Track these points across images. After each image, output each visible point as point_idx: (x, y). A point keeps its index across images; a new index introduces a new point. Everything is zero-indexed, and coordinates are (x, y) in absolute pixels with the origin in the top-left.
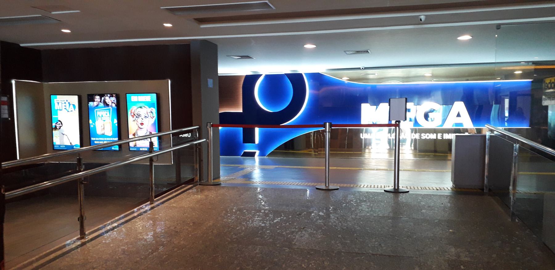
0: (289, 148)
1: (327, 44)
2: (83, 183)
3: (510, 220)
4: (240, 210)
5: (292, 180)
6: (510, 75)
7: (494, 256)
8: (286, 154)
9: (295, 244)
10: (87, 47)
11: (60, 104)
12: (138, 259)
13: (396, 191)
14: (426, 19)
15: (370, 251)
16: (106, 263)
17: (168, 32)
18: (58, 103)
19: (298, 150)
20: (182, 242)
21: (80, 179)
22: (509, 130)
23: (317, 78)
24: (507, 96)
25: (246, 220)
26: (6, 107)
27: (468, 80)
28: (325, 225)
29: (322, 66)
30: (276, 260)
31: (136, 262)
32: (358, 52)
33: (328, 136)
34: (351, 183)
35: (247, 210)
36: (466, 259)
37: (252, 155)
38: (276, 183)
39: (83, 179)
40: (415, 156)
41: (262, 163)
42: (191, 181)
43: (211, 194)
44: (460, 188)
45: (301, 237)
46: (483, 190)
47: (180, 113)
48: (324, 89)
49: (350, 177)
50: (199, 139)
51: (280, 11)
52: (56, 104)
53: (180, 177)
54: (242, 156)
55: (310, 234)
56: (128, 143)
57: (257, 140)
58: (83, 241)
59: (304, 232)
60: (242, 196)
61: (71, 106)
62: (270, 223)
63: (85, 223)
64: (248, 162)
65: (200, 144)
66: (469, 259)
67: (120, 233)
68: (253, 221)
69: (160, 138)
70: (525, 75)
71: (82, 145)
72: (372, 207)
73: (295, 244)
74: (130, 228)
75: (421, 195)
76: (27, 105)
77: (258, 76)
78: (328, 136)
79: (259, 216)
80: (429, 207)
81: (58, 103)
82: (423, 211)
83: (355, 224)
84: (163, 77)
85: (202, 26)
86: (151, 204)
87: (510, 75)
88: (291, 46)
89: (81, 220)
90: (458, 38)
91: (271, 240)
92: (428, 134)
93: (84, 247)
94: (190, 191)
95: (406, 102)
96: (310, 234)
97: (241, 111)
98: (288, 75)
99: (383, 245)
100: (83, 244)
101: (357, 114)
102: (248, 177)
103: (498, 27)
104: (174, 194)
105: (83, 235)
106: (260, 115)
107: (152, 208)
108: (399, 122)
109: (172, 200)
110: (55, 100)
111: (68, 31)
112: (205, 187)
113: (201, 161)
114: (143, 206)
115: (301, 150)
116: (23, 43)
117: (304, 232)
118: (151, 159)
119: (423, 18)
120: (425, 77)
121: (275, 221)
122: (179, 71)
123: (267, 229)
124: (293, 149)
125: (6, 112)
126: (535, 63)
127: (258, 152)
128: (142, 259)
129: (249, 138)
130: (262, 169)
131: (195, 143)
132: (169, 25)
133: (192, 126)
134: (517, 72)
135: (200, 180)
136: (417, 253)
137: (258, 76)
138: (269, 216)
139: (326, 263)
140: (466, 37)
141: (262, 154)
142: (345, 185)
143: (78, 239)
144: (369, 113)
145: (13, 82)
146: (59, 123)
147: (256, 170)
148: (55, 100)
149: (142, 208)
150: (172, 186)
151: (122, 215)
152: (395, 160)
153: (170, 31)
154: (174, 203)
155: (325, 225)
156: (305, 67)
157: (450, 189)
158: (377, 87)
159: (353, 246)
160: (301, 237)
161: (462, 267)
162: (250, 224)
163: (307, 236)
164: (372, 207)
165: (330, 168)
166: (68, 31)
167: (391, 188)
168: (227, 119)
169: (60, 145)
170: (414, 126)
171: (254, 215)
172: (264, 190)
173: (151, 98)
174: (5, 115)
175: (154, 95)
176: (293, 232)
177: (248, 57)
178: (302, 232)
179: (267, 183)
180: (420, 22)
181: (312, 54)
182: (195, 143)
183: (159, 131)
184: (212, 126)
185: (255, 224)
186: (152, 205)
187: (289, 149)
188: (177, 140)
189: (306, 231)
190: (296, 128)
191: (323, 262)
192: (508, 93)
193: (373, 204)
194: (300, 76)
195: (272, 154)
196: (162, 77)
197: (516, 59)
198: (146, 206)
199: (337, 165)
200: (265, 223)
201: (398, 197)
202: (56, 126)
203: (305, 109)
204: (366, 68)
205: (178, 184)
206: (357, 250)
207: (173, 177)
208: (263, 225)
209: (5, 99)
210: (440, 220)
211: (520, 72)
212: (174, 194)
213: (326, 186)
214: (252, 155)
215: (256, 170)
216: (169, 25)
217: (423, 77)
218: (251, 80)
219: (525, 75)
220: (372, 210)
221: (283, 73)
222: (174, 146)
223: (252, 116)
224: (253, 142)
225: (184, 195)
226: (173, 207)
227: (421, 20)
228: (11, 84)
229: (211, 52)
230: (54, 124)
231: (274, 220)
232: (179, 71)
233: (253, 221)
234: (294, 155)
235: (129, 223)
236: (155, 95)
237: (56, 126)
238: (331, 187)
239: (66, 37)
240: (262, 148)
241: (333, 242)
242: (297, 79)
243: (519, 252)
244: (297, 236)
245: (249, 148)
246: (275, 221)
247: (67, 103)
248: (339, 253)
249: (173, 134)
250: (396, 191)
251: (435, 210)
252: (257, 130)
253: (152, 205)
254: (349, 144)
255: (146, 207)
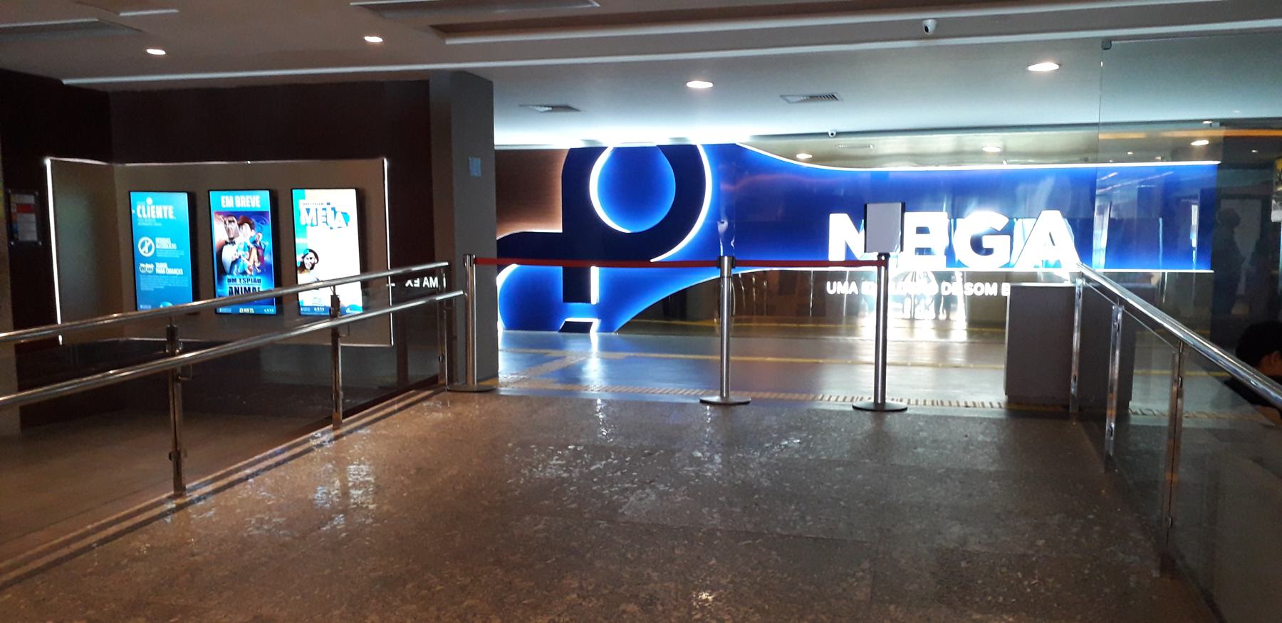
0: (677, 314)
1: (741, 81)
2: (178, 381)
3: (1102, 471)
4: (524, 445)
5: (670, 383)
6: (1180, 150)
7: (1040, 542)
8: (668, 329)
9: (623, 514)
10: (294, 81)
11: (312, 212)
12: (287, 539)
13: (880, 408)
14: (937, 26)
15: (778, 530)
16: (220, 545)
17: (373, 55)
18: (308, 210)
19: (693, 320)
20: (385, 508)
21: (174, 370)
22: (1118, 278)
23: (729, 155)
24: (1195, 197)
25: (530, 464)
26: (33, 217)
27: (1086, 161)
28: (698, 476)
29: (741, 129)
30: (574, 544)
31: (283, 545)
32: (813, 98)
33: (727, 286)
34: (809, 392)
35: (538, 445)
36: (977, 548)
37: (585, 328)
38: (630, 389)
39: (179, 370)
40: (971, 334)
41: (606, 346)
42: (430, 383)
43: (473, 410)
44: (1018, 404)
45: (641, 499)
46: (1067, 407)
47: (405, 234)
48: (745, 181)
49: (803, 380)
50: (449, 290)
51: (607, 11)
52: (303, 212)
53: (406, 375)
54: (562, 331)
55: (661, 495)
56: (296, 294)
57: (595, 295)
58: (179, 501)
59: (648, 490)
60: (534, 416)
61: (339, 215)
62: (581, 472)
63: (186, 464)
64: (574, 346)
65: (449, 300)
66: (985, 549)
67: (259, 486)
68: (544, 467)
69: (365, 285)
70: (1208, 153)
71: (366, 308)
72: (809, 442)
73: (623, 514)
74: (283, 478)
75: (924, 416)
76: (79, 211)
77: (600, 150)
78: (727, 286)
79: (561, 457)
80: (935, 441)
81: (308, 210)
82: (920, 450)
83: (763, 473)
84: (374, 154)
85: (449, 42)
86: (334, 429)
87: (1180, 150)
88: (660, 86)
89: (176, 457)
90: (1031, 68)
91: (573, 506)
92: (979, 284)
93: (182, 512)
94: (425, 404)
95: (903, 211)
96: (661, 495)
97: (558, 229)
98: (665, 149)
99: (808, 518)
100: (180, 507)
101: (820, 237)
102: (572, 376)
103: (1107, 44)
104: (396, 407)
105: (180, 489)
106: (581, 240)
107: (337, 438)
108: (887, 256)
109: (382, 423)
110: (301, 202)
111: (161, 52)
112: (459, 395)
113: (452, 339)
114: (318, 433)
115: (701, 319)
116: (67, 77)
117: (648, 490)
118: (334, 332)
119: (930, 24)
120: (991, 154)
121: (593, 468)
122: (405, 143)
123: (571, 484)
124: (683, 316)
125: (34, 227)
126: (1225, 123)
127: (596, 323)
128: (294, 538)
129: (577, 290)
130: (608, 362)
131: (439, 298)
132: (375, 40)
133: (433, 261)
134: (1197, 144)
135: (451, 380)
136: (877, 535)
137: (600, 150)
138: (583, 458)
139: (677, 552)
140: (1047, 67)
141: (606, 327)
142: (789, 396)
143: (170, 498)
144: (842, 233)
145: (48, 162)
146: (311, 255)
147: (592, 361)
148: (301, 202)
149: (313, 438)
150: (385, 394)
151: (270, 451)
152: (913, 338)
153: (377, 52)
154: (384, 428)
155: (698, 476)
156: (705, 131)
157: (995, 405)
158: (891, 176)
159: (745, 519)
160: (641, 499)
161: (963, 564)
162: (538, 474)
163: (653, 497)
164: (809, 442)
165: (731, 358)
166: (161, 52)
167: (868, 399)
168: (515, 249)
169: (312, 308)
170: (948, 265)
171: (550, 456)
172: (608, 403)
173: (346, 199)
174: (31, 235)
175: (183, 199)
176: (627, 489)
177: (567, 108)
178: (644, 489)
179: (617, 388)
180: (923, 33)
181: (1048, 85)
182: (439, 298)
183: (364, 269)
184: (476, 261)
185: (550, 473)
186: (338, 432)
187: (674, 317)
188: (402, 294)
189: (653, 488)
190: (679, 267)
191: (673, 548)
192: (1197, 192)
193: (814, 435)
194: (692, 150)
195: (628, 327)
196: (371, 152)
197: (1198, 112)
198: (323, 433)
199: (767, 351)
200: (570, 472)
201: (882, 420)
202: (302, 263)
203: (705, 225)
204: (839, 134)
205: (402, 387)
206: (749, 527)
207: (387, 373)
208: (565, 475)
209: (30, 200)
210: (948, 469)
211: (1206, 142)
212: (396, 407)
213: (721, 395)
214: (585, 328)
215: (592, 361)
216: (375, 40)
217: (978, 155)
218: (581, 159)
219: (1208, 153)
220: (808, 446)
221: (654, 144)
222: (396, 303)
223: (583, 242)
224: (587, 299)
225: (412, 411)
226: (381, 435)
227: (927, 29)
228: (45, 168)
229: (478, 97)
230: (299, 259)
231: (592, 465)
232: (405, 143)
233: (544, 467)
234: (685, 330)
235: (282, 467)
236: (267, 193)
237: (302, 263)
238: (734, 398)
239: (157, 64)
240: (607, 312)
241: (705, 510)
242: (684, 157)
243: (1095, 536)
244: (632, 499)
245: (577, 315)
246: (593, 468)
247: (329, 208)
248: (711, 533)
249: (394, 278)
250: (880, 408)
251: (944, 448)
252: (595, 273)
253: (338, 432)
254: (800, 309)
255: (322, 436)
